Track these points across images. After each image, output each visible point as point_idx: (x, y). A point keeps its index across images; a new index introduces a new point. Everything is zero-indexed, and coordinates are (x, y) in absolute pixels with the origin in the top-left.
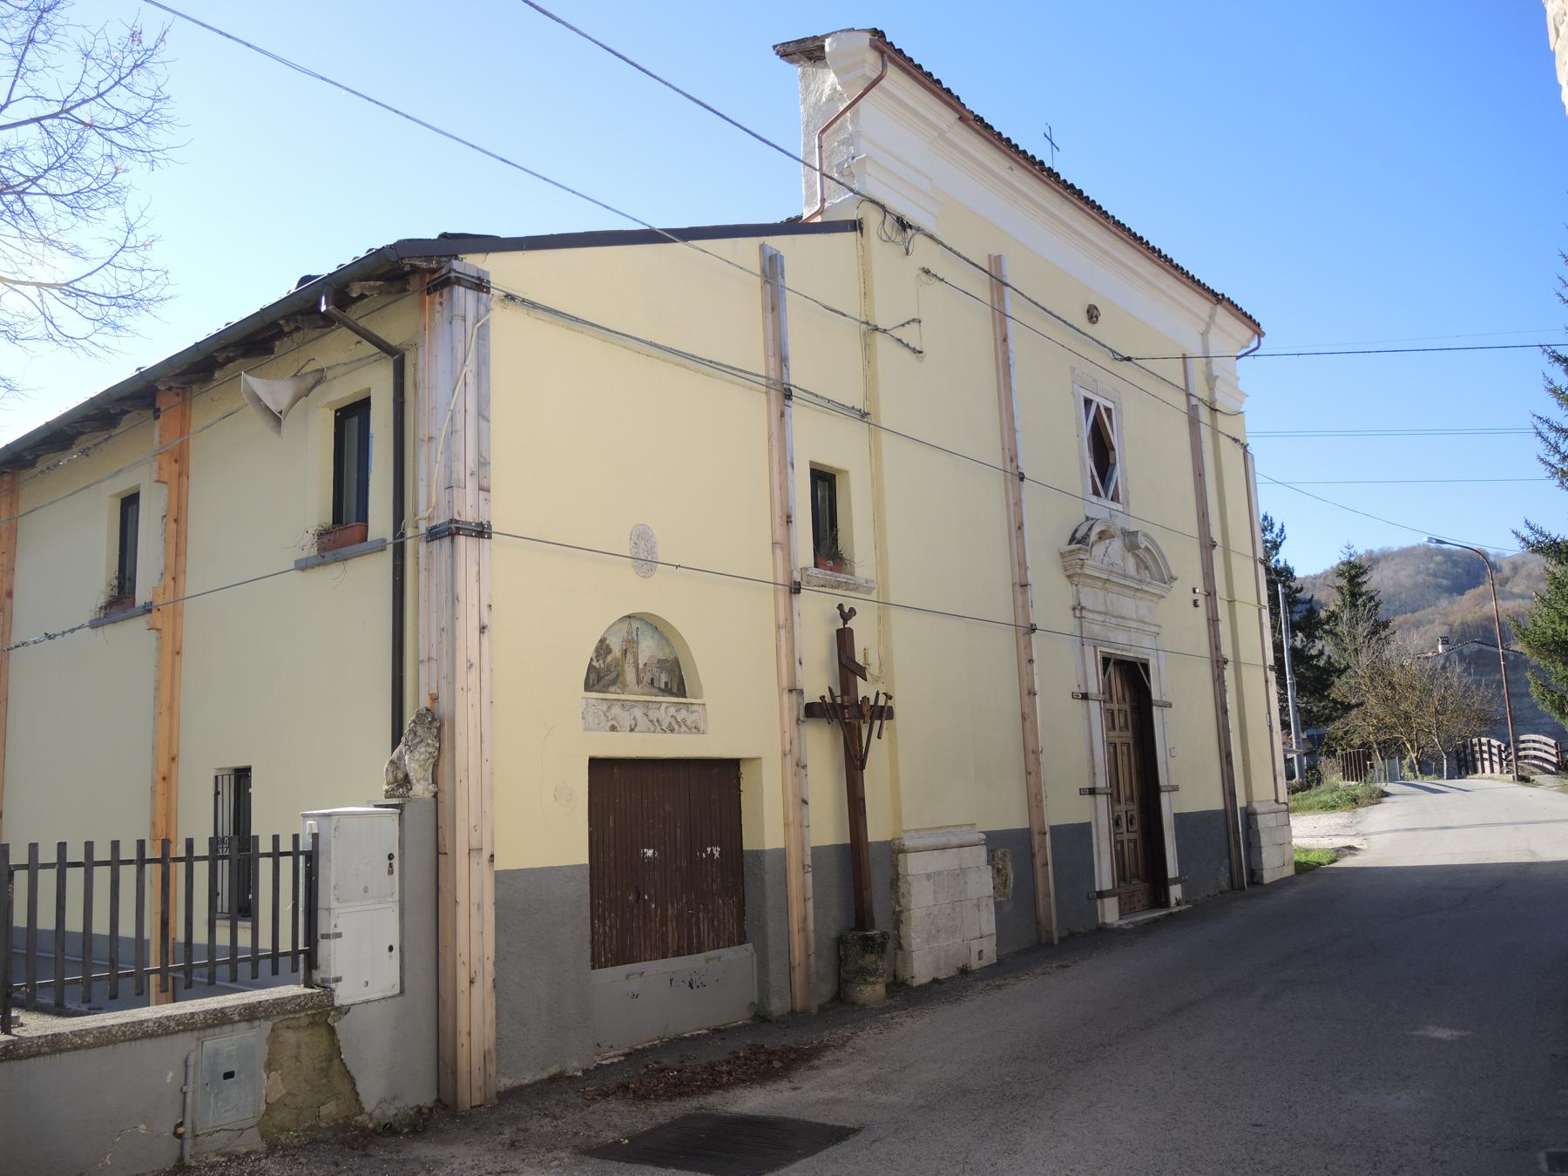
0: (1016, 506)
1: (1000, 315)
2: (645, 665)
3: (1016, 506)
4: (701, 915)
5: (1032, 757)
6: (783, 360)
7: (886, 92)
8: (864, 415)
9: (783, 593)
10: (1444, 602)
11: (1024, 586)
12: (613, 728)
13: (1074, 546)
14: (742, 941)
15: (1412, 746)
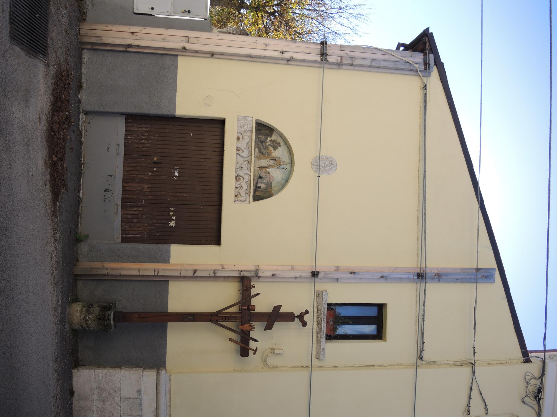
2: (269, 173)
4: (141, 209)
12: (238, 139)
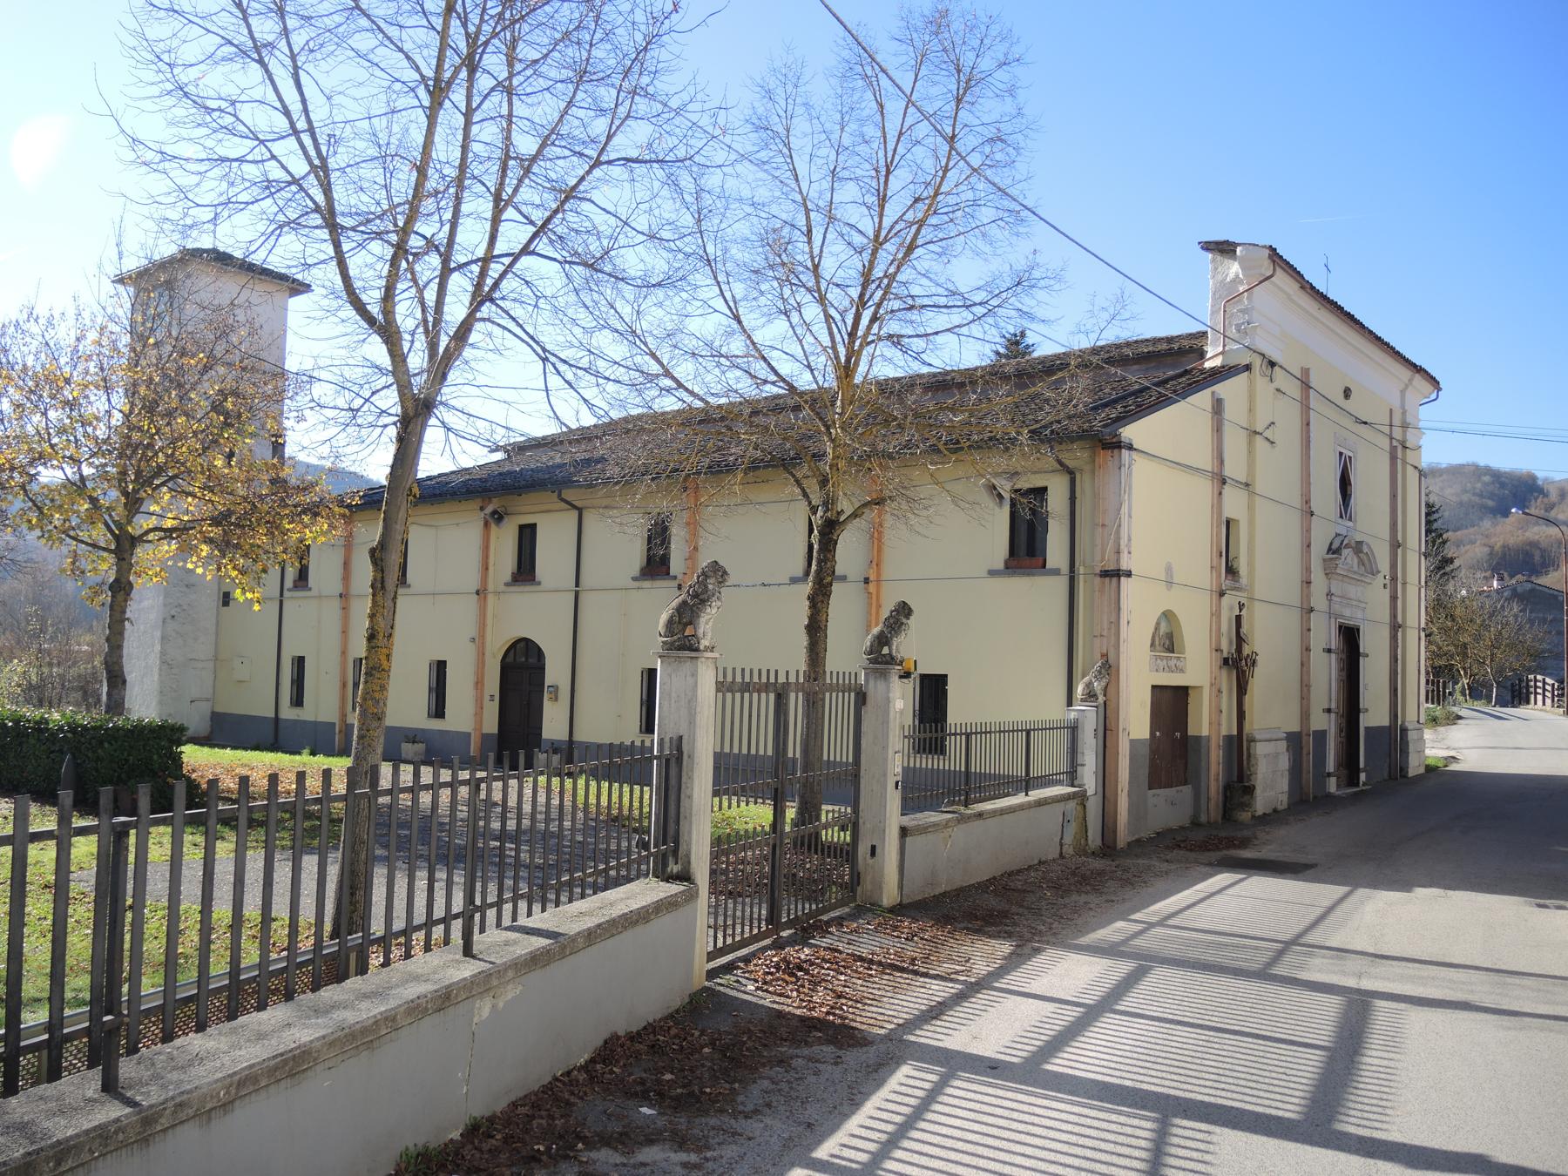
0: (1307, 530)
1: (1306, 408)
3: (1307, 530)
5: (1305, 689)
6: (1222, 462)
7: (1275, 284)
8: (1247, 485)
9: (1215, 596)
10: (1487, 524)
11: (1309, 583)
13: (1330, 556)
14: (1185, 783)
15: (1466, 673)
